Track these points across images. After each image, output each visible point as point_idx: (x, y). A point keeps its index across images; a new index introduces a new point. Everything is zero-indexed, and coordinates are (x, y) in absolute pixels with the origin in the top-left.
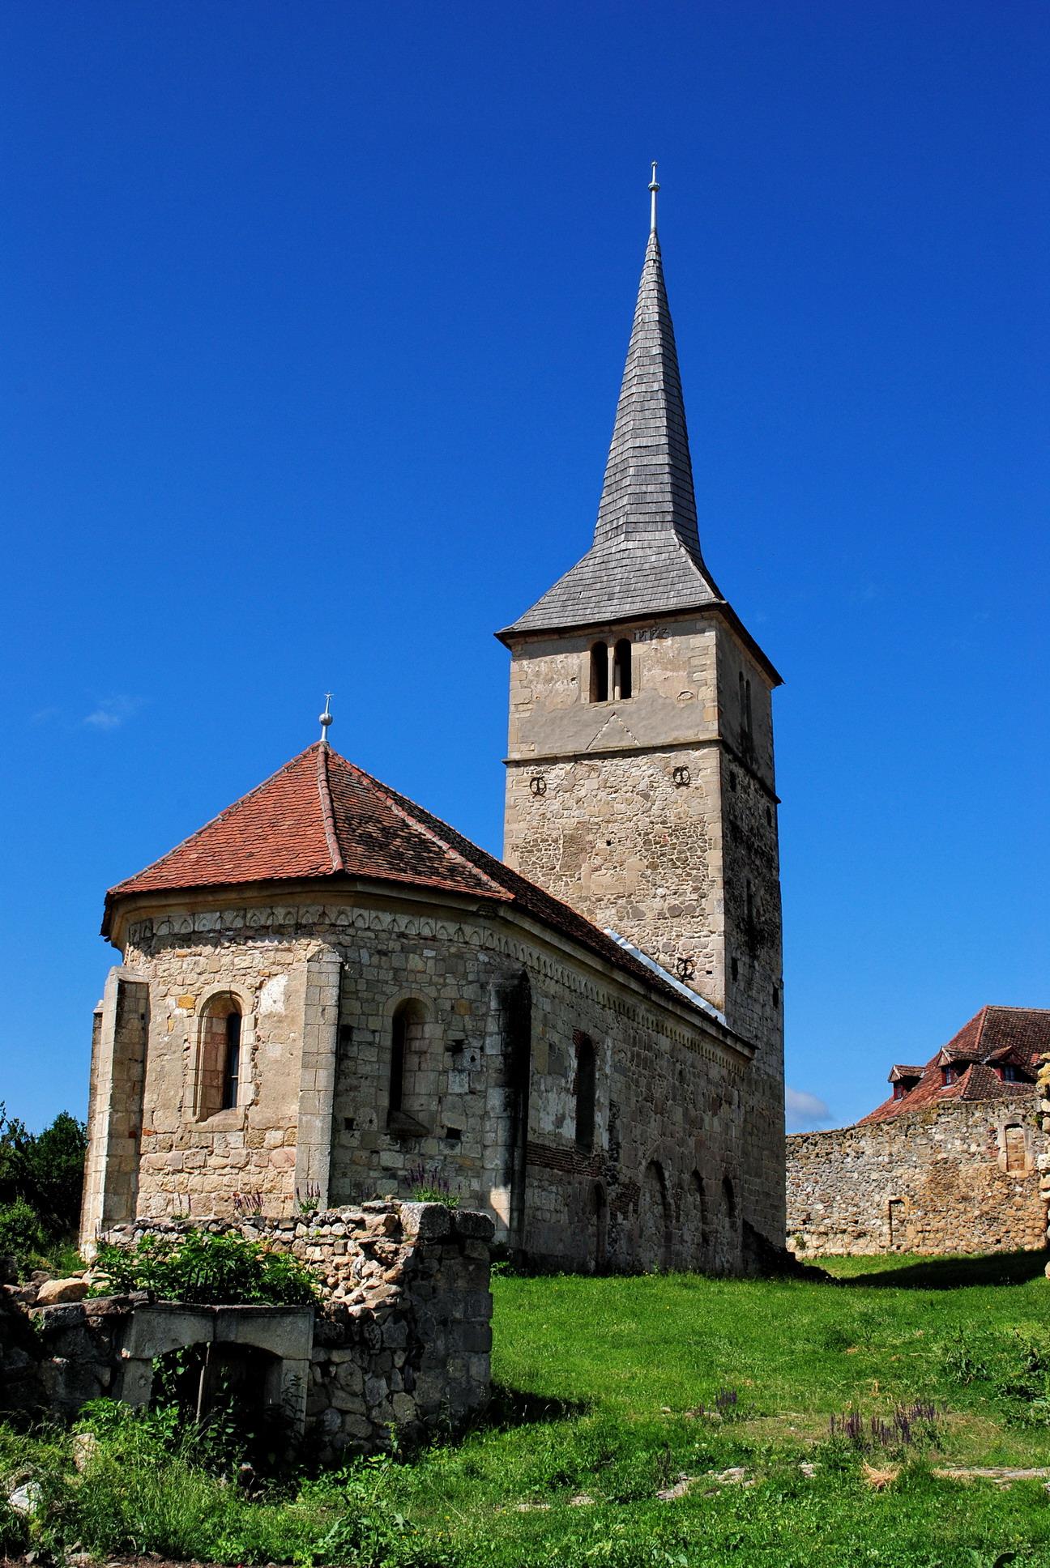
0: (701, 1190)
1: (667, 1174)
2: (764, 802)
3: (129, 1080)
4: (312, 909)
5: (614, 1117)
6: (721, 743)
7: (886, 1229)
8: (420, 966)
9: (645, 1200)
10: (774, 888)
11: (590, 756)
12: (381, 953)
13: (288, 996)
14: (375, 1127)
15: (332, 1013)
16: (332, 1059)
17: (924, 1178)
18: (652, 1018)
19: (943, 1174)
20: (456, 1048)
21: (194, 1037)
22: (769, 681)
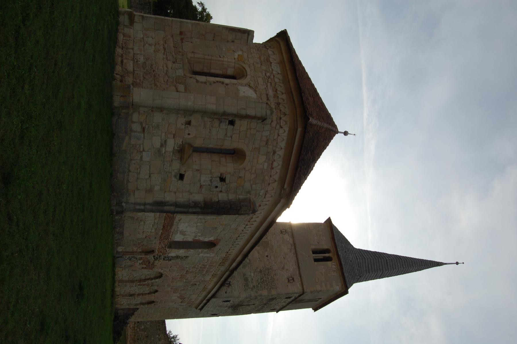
0: (150, 293)
1: (157, 280)
5: (181, 258)
12: (267, 141)
14: (186, 136)
18: (219, 273)
20: (222, 179)
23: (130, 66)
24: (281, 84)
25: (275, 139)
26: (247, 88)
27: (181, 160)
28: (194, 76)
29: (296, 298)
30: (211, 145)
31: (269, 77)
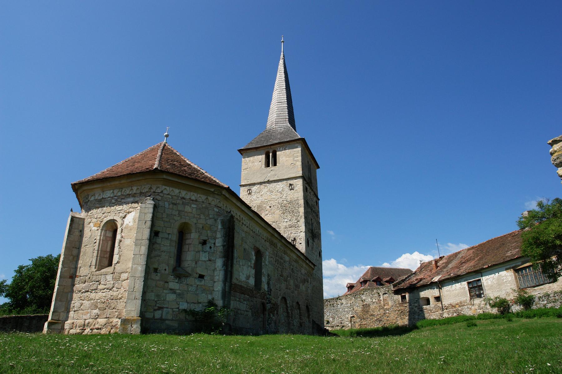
0: (299, 308)
1: (288, 302)
2: (315, 199)
3: (72, 255)
4: (146, 187)
6: (303, 177)
7: (350, 325)
8: (190, 210)
9: (281, 311)
10: (319, 223)
11: (264, 182)
13: (134, 220)
15: (149, 224)
16: (147, 242)
17: (360, 309)
19: (366, 307)
20: (204, 243)
21: (98, 238)
22: (316, 167)
23: (102, 321)
24: (123, 191)
25: (172, 198)
26: (125, 220)
27: (187, 277)
28: (113, 265)
29: (307, 183)
30: (174, 250)
31: (116, 200)
